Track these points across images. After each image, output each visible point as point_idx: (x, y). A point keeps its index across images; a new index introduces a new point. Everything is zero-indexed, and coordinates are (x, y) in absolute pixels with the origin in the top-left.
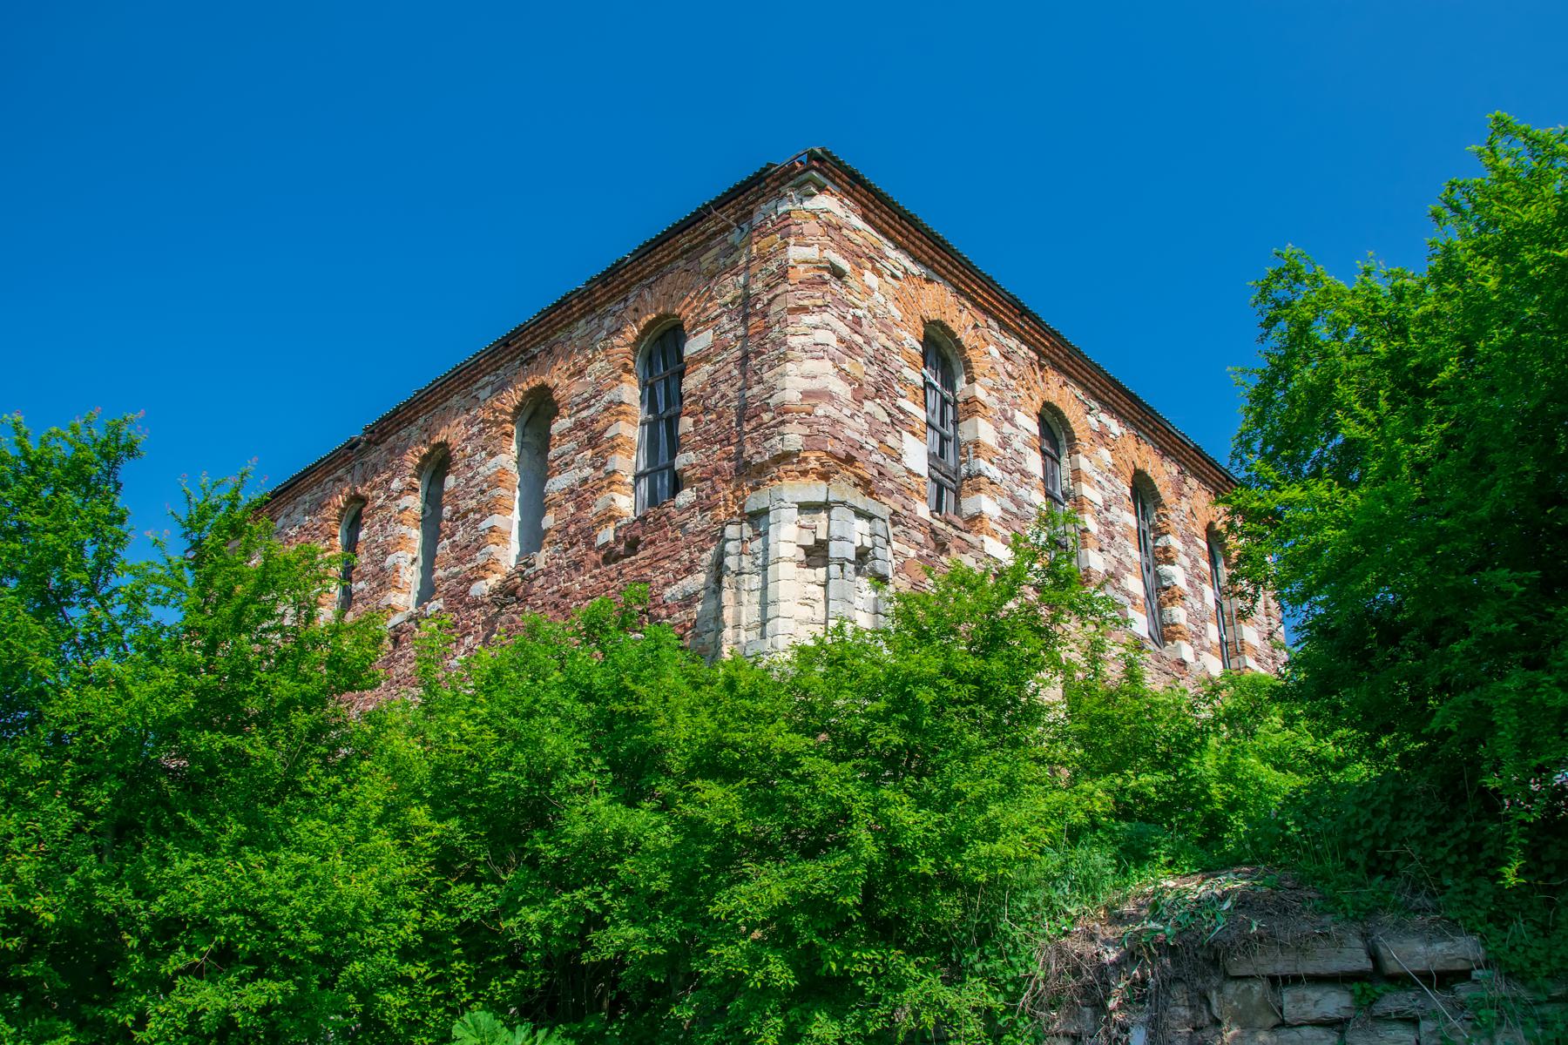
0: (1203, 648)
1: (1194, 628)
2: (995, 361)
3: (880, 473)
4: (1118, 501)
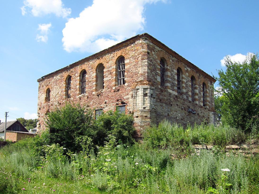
0: (200, 102)
1: (199, 99)
2: (171, 62)
3: (154, 82)
4: (189, 81)
